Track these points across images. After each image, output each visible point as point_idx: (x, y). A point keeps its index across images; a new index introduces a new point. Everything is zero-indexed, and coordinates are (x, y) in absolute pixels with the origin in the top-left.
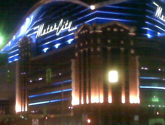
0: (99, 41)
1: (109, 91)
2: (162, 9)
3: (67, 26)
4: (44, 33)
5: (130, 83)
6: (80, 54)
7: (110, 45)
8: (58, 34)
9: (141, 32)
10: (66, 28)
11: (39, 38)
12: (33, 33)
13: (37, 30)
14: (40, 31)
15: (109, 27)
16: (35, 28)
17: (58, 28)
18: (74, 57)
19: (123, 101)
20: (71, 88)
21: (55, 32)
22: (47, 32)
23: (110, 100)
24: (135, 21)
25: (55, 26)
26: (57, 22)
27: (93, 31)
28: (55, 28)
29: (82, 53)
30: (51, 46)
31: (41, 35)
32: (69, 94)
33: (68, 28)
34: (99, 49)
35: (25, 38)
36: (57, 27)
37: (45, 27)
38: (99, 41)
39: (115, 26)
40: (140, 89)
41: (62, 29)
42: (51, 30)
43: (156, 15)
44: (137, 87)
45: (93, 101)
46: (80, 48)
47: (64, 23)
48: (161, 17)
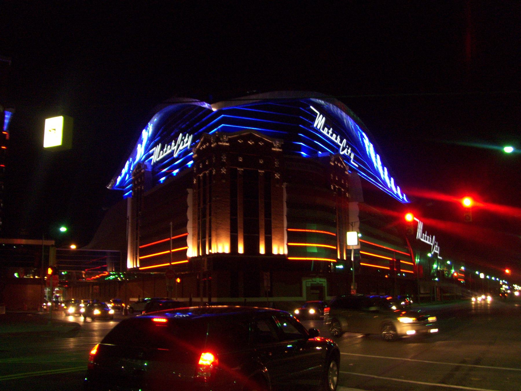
0: (224, 159)
1: (260, 239)
2: (324, 118)
3: (187, 142)
4: (161, 157)
5: (274, 223)
6: (198, 179)
7: (241, 165)
8: (175, 155)
9: (291, 149)
10: (185, 146)
11: (157, 163)
12: (287, 216)
13: (152, 154)
14: (158, 155)
15: (240, 138)
16: (151, 151)
17: (176, 147)
18: (192, 186)
19: (262, 250)
20: (186, 232)
21: (172, 153)
22: (165, 155)
23: (241, 249)
24: (407, 240)
25: (173, 144)
26: (176, 138)
27: (215, 144)
28: (173, 148)
29: (201, 178)
30: (168, 174)
31: (158, 160)
32: (183, 242)
33: (187, 144)
34: (224, 171)
35: (140, 165)
36: (175, 145)
37: (162, 149)
38: (224, 159)
39: (251, 137)
40: (289, 233)
41: (181, 148)
42: (169, 152)
43: (315, 125)
44: (283, 230)
45: (214, 250)
46: (199, 171)
47: (183, 138)
48: (323, 129)
